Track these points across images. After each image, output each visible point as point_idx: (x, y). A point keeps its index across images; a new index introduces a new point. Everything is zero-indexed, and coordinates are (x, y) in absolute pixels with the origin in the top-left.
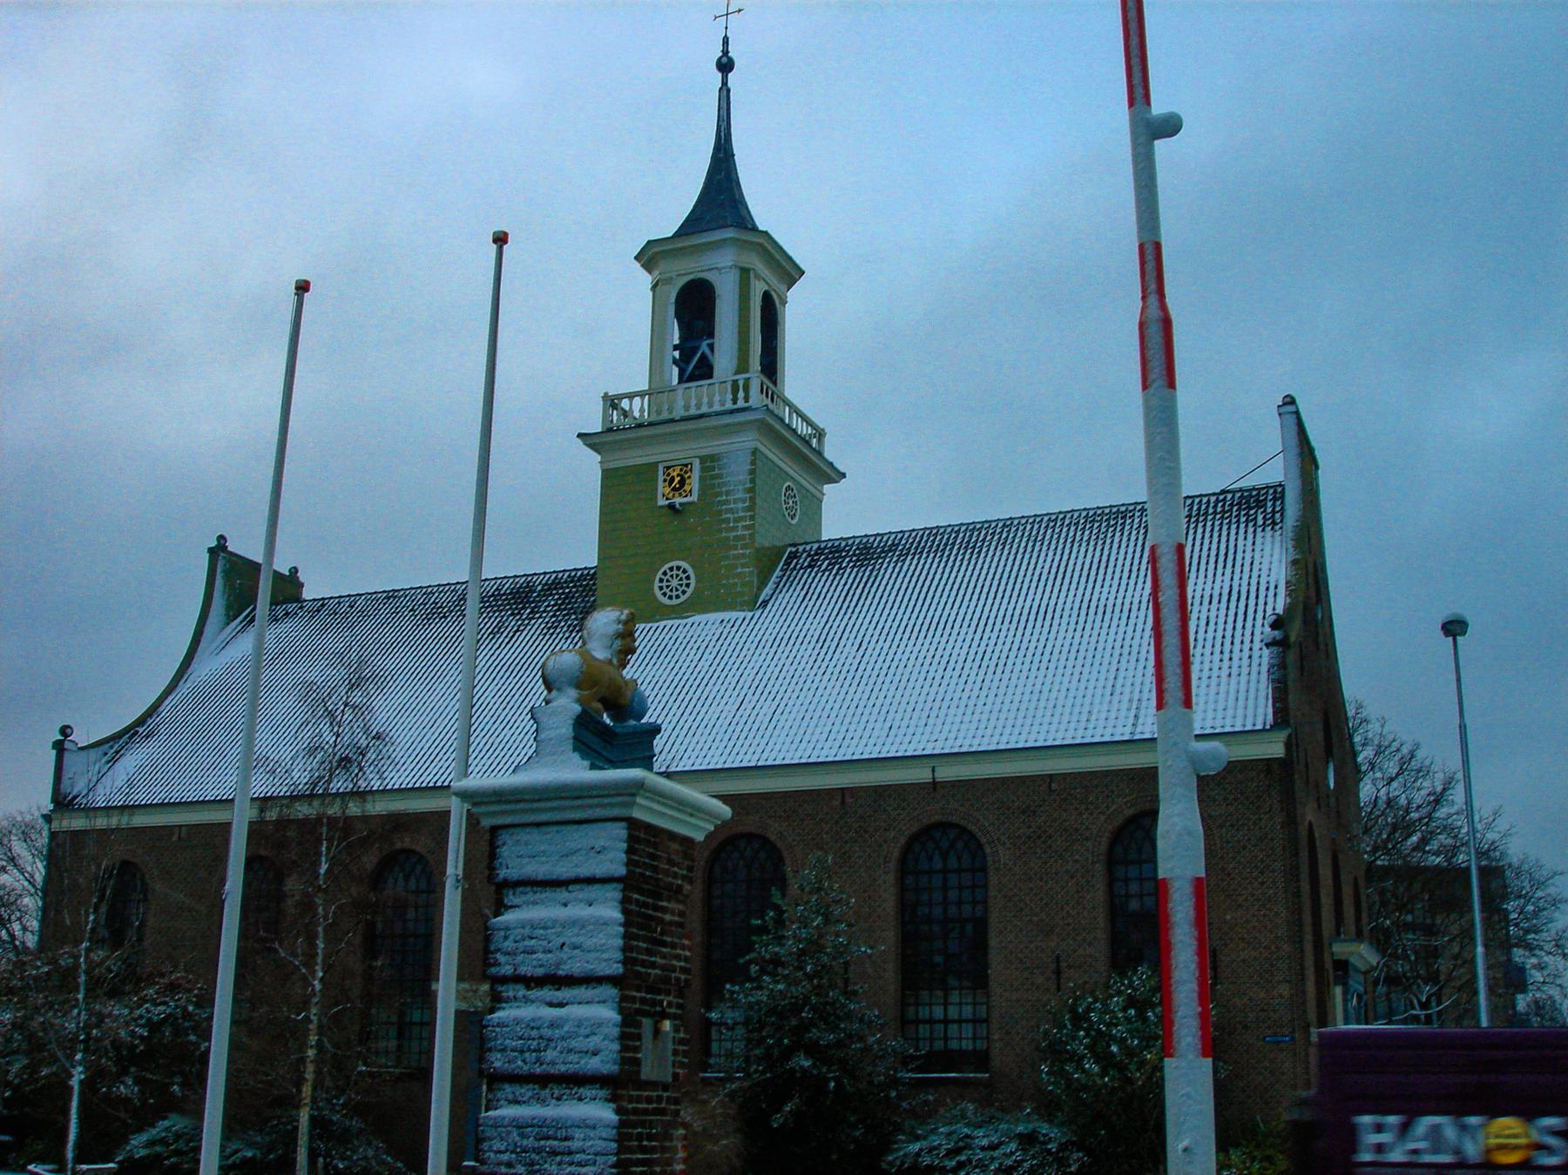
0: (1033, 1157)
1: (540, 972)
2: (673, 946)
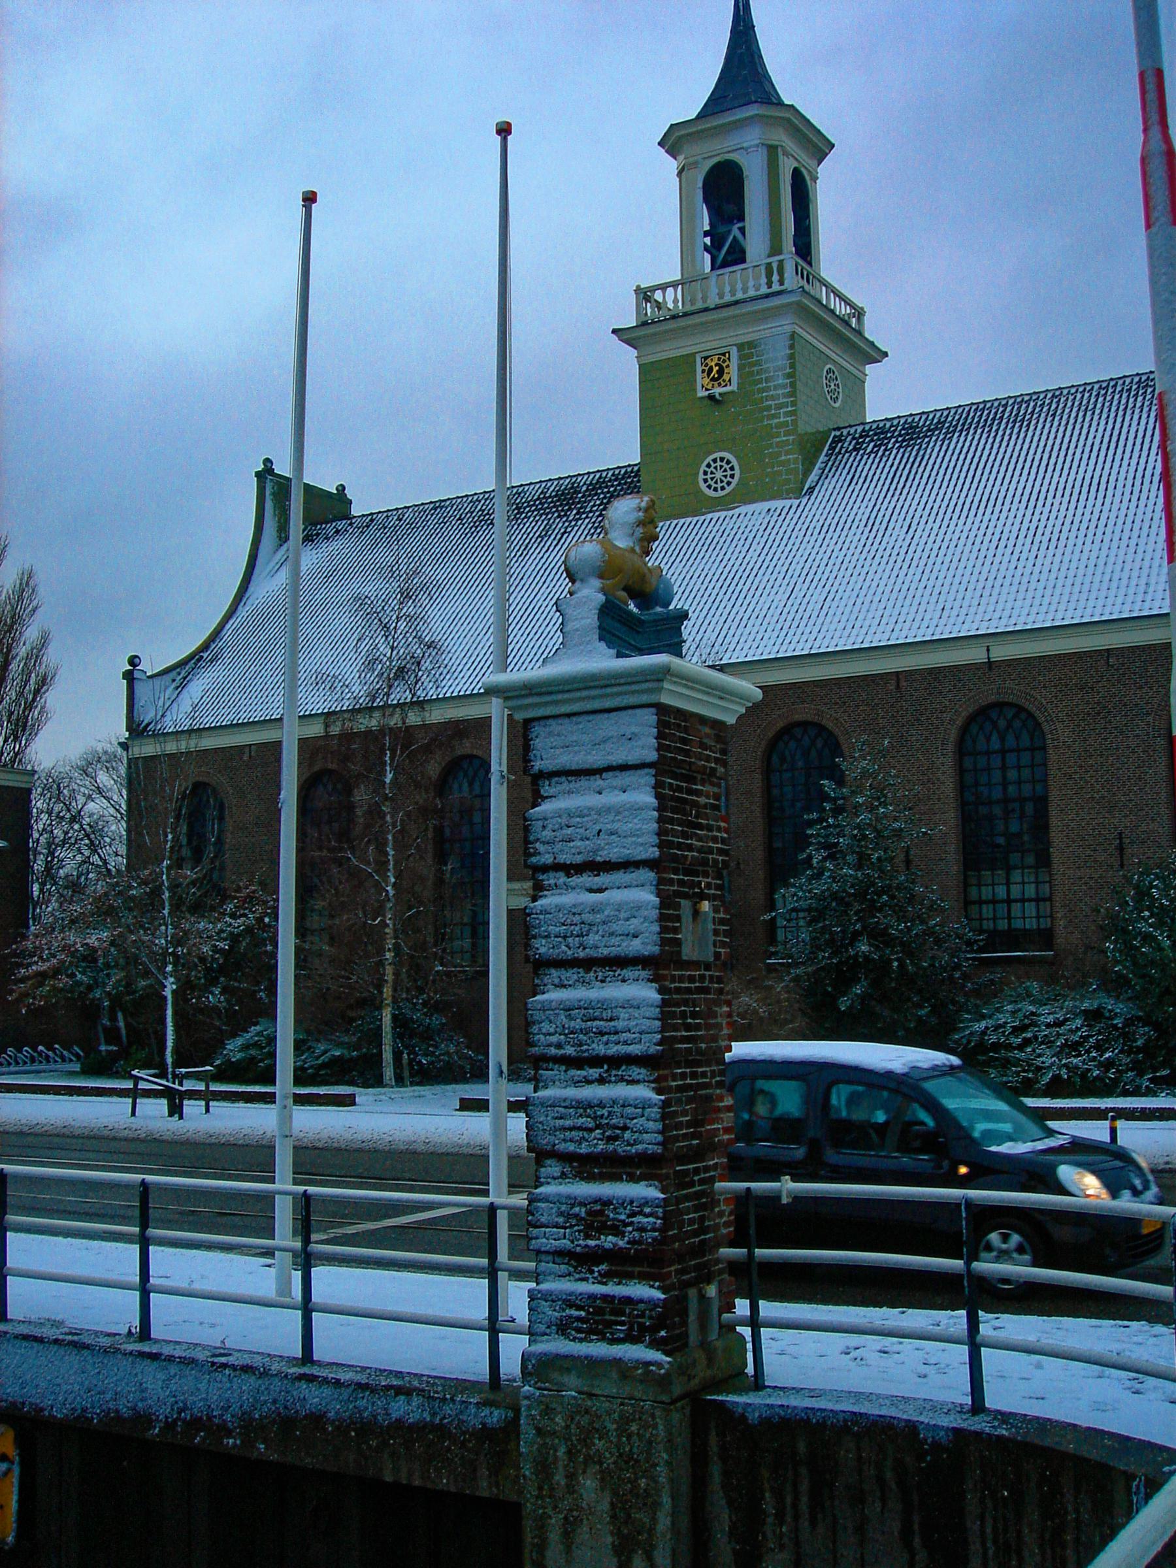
0: (1100, 1033)
1: (579, 859)
2: (709, 828)
